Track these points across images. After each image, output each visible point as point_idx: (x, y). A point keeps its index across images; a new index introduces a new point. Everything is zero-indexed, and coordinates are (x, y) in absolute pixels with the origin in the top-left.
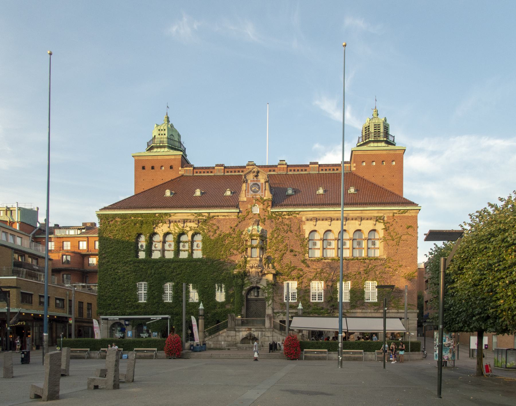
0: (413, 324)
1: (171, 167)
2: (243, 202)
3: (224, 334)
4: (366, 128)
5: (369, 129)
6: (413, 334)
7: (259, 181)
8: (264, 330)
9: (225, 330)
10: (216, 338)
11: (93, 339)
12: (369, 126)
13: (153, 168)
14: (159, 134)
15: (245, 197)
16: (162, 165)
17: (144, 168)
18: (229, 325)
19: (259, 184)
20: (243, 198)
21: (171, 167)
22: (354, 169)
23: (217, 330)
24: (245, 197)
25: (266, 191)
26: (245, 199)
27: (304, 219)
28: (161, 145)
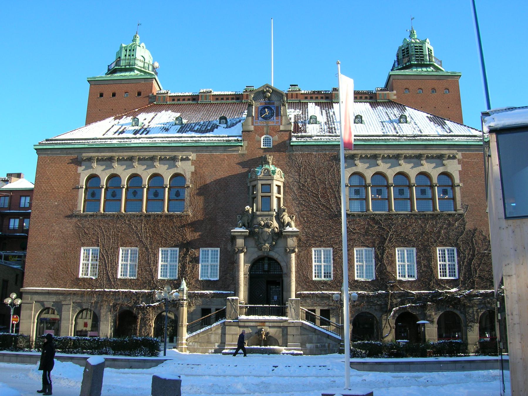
7: (274, 104)
12: (408, 48)
15: (253, 124)
22: (395, 97)
24: (253, 124)
28: (128, 67)
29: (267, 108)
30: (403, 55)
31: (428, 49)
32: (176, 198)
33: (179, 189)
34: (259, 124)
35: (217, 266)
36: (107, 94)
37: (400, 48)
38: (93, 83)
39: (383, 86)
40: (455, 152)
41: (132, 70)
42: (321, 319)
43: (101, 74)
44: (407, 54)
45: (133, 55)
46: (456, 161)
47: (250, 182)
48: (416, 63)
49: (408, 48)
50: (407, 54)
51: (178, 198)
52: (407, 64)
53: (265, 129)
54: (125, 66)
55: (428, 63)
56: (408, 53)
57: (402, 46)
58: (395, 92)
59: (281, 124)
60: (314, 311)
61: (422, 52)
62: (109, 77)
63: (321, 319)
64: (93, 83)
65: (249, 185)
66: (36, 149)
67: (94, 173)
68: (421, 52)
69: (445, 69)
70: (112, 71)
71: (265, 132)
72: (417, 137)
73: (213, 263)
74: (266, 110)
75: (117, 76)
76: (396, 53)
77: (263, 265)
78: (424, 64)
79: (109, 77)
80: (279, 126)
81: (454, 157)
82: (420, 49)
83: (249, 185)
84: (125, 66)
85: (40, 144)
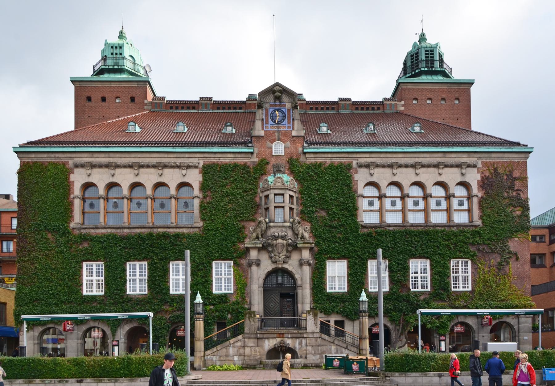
0: (526, 322)
1: (132, 99)
2: (259, 137)
3: (239, 344)
4: (412, 56)
5: (418, 56)
6: (526, 338)
7: (285, 106)
8: (305, 336)
9: (240, 337)
10: (224, 350)
11: (25, 357)
12: (417, 53)
13: (104, 99)
14: (112, 54)
15: (263, 129)
16: (119, 95)
17: (89, 99)
18: (246, 330)
19: (284, 110)
20: (259, 131)
21: (132, 99)
22: (403, 108)
23: (223, 339)
24: (263, 129)
25: (296, 122)
26: (262, 133)
27: (354, 164)
28: (116, 67)
29: (278, 110)
30: (412, 62)
31: (439, 53)
32: (185, 210)
33: (188, 201)
34: (269, 129)
35: (230, 279)
36: (96, 98)
37: (408, 54)
38: (79, 84)
39: (389, 96)
40: (474, 159)
41: (121, 71)
42: (335, 328)
43: (87, 73)
44: (416, 60)
45: (121, 54)
46: (475, 170)
47: (262, 192)
48: (426, 69)
49: (417, 53)
50: (416, 60)
51: (186, 210)
52: (417, 71)
53: (276, 134)
54: (114, 66)
55: (439, 69)
56: (418, 59)
57: (411, 51)
58: (403, 102)
59: (293, 129)
60: (329, 321)
61: (433, 57)
62: (96, 78)
63: (335, 328)
64: (79, 84)
65: (261, 195)
66: (16, 152)
67: (90, 181)
68: (431, 57)
69: (457, 75)
70: (101, 72)
71: (277, 138)
72: (169, 228)
73: (227, 277)
74: (277, 112)
75: (106, 77)
76: (403, 61)
77: (277, 278)
78: (435, 71)
79: (96, 78)
80: (291, 131)
81: (475, 166)
82: (431, 54)
83: (261, 195)
84: (114, 66)
85: (21, 146)
